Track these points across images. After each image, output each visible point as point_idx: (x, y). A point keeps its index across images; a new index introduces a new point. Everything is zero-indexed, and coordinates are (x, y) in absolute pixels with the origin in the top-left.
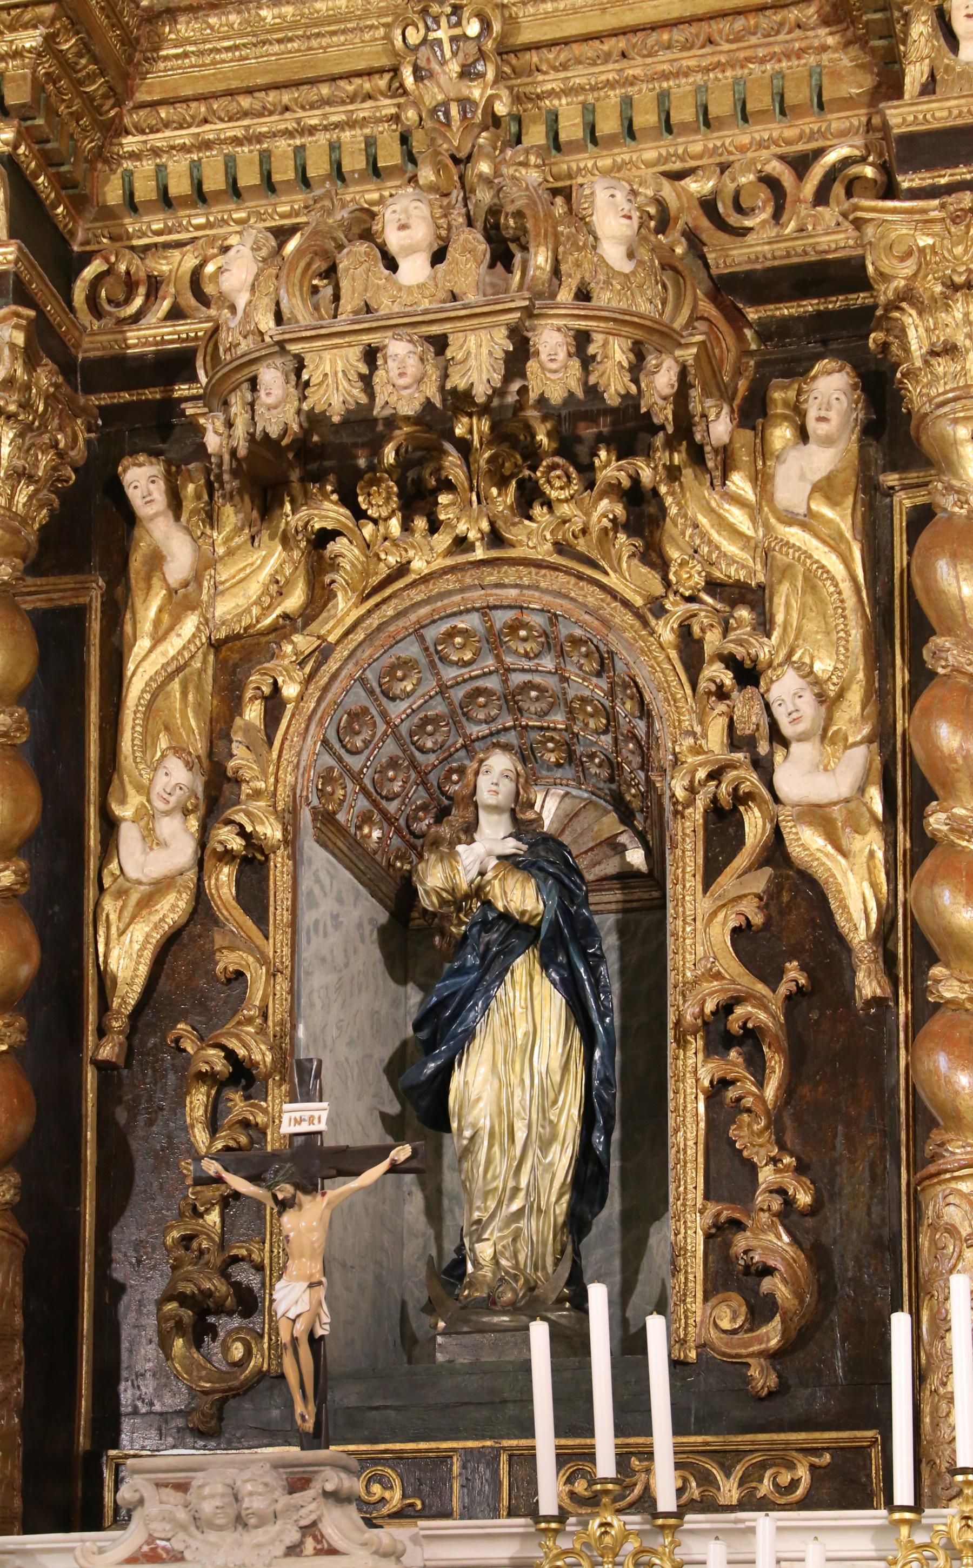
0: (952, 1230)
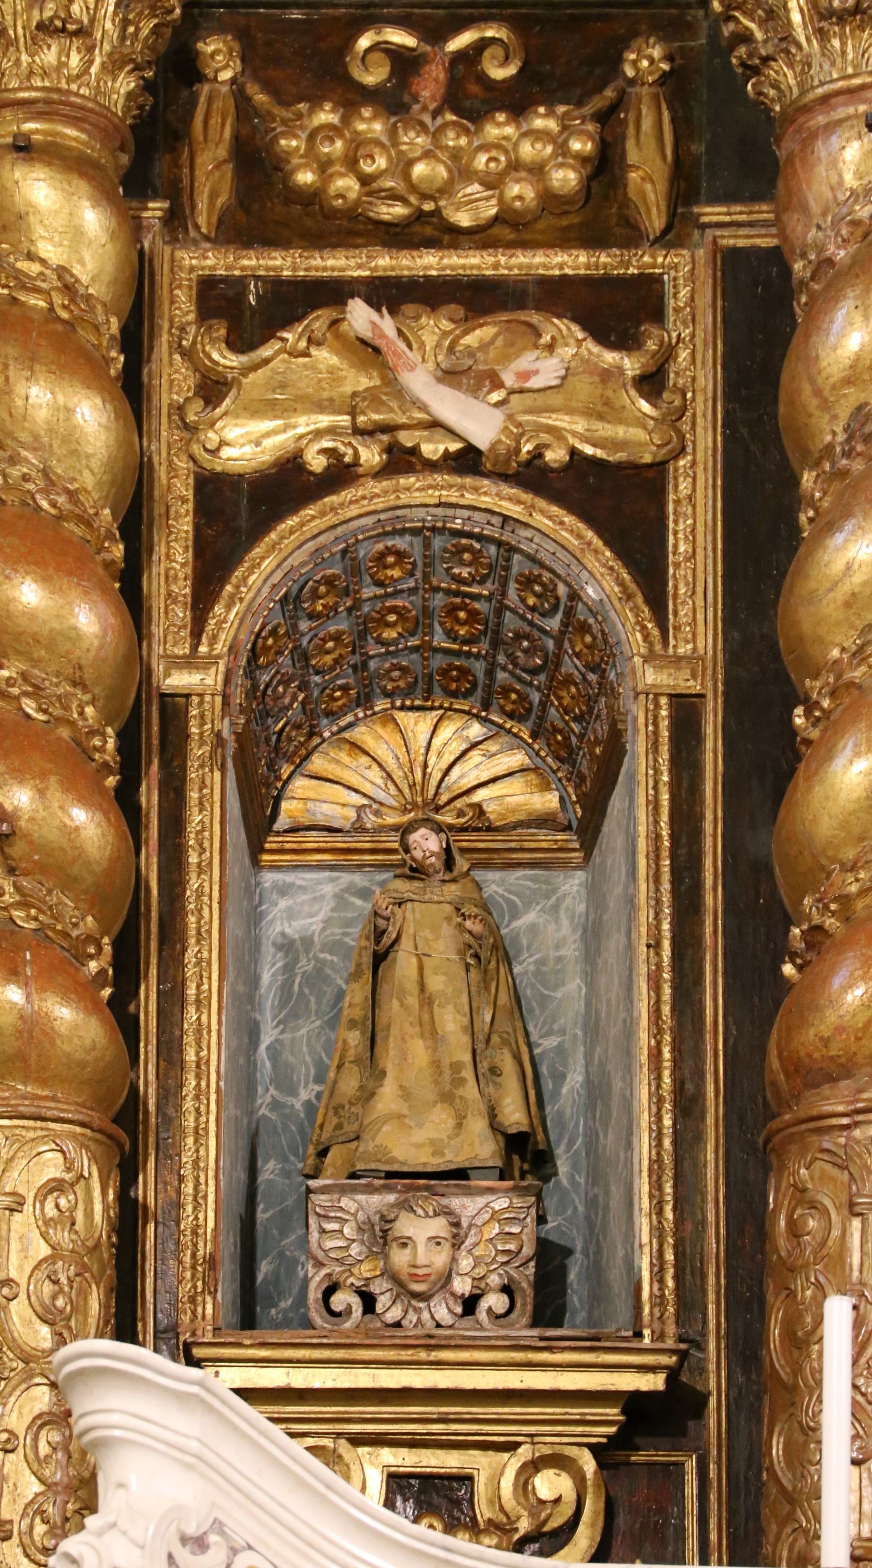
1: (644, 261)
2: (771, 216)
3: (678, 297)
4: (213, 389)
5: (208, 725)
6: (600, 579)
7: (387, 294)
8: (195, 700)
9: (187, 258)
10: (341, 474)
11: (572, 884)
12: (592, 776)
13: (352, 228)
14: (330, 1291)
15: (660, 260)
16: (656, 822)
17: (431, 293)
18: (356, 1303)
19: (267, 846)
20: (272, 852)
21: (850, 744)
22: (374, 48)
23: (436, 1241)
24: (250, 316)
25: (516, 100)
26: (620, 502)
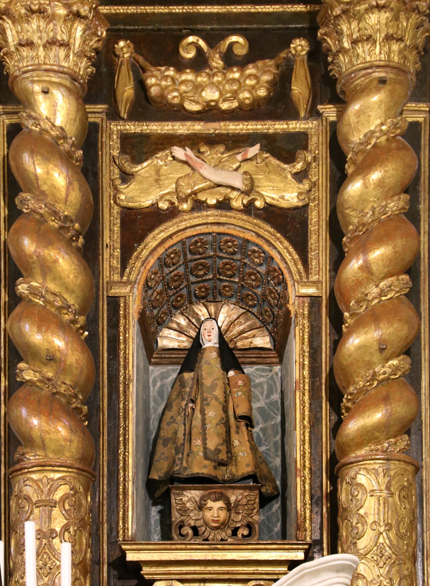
0: (28, 499)
1: (294, 126)
2: (89, 115)
3: (313, 142)
4: (126, 177)
5: (134, 306)
6: (282, 251)
7: (192, 141)
8: (122, 300)
9: (116, 127)
10: (173, 213)
11: (277, 368)
12: (280, 329)
13: (179, 113)
14: (181, 527)
15: (298, 126)
16: (125, 474)
17: (212, 141)
18: (190, 532)
19: (154, 356)
20: (155, 358)
21: (187, 473)
22: (193, 43)
23: (221, 509)
24: (139, 148)
25: (242, 63)
26: (289, 223)
